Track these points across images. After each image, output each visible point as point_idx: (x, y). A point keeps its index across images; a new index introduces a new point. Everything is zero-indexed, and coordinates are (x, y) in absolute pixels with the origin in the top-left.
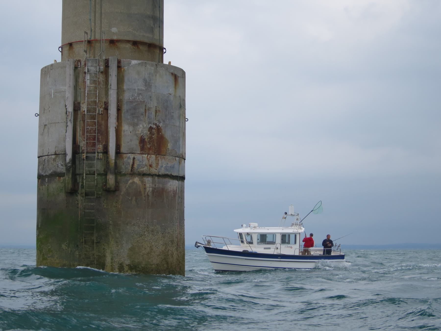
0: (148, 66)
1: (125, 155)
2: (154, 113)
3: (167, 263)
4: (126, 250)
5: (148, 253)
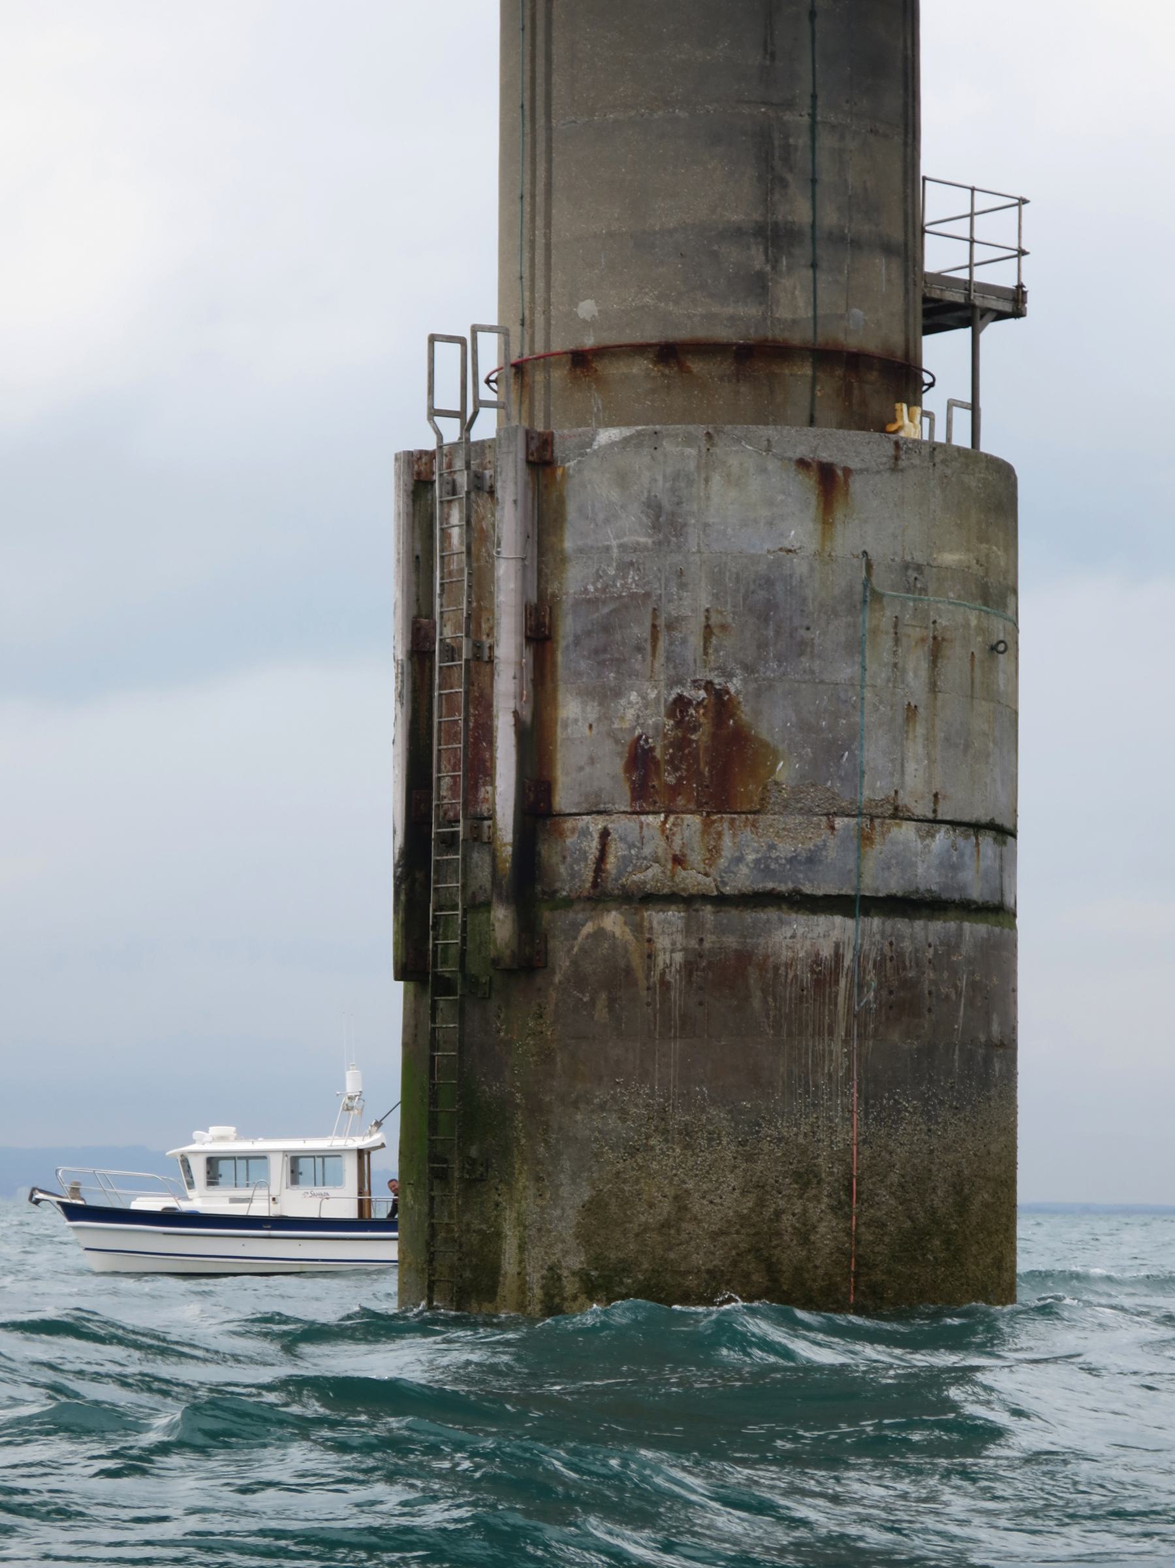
0: (668, 446)
1: (569, 824)
2: (695, 641)
4: (570, 1212)
5: (665, 1225)
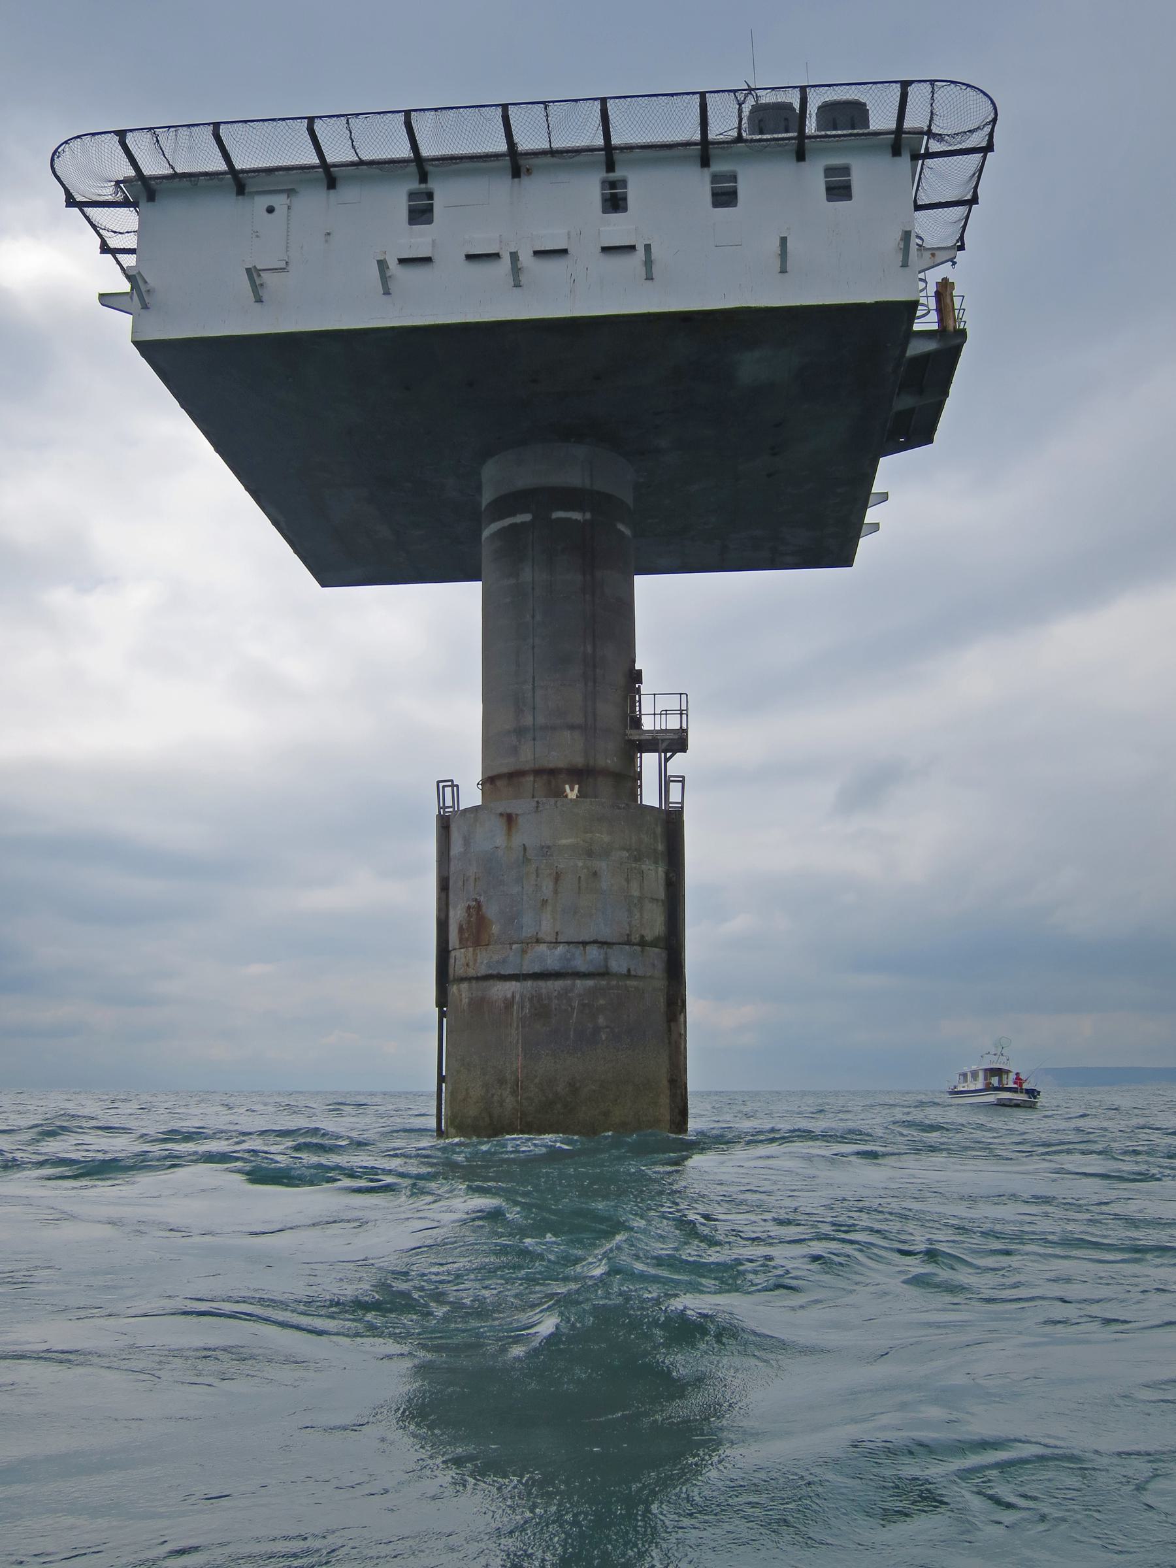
3: (491, 1116)
